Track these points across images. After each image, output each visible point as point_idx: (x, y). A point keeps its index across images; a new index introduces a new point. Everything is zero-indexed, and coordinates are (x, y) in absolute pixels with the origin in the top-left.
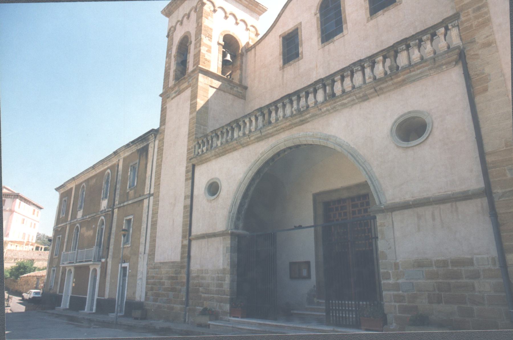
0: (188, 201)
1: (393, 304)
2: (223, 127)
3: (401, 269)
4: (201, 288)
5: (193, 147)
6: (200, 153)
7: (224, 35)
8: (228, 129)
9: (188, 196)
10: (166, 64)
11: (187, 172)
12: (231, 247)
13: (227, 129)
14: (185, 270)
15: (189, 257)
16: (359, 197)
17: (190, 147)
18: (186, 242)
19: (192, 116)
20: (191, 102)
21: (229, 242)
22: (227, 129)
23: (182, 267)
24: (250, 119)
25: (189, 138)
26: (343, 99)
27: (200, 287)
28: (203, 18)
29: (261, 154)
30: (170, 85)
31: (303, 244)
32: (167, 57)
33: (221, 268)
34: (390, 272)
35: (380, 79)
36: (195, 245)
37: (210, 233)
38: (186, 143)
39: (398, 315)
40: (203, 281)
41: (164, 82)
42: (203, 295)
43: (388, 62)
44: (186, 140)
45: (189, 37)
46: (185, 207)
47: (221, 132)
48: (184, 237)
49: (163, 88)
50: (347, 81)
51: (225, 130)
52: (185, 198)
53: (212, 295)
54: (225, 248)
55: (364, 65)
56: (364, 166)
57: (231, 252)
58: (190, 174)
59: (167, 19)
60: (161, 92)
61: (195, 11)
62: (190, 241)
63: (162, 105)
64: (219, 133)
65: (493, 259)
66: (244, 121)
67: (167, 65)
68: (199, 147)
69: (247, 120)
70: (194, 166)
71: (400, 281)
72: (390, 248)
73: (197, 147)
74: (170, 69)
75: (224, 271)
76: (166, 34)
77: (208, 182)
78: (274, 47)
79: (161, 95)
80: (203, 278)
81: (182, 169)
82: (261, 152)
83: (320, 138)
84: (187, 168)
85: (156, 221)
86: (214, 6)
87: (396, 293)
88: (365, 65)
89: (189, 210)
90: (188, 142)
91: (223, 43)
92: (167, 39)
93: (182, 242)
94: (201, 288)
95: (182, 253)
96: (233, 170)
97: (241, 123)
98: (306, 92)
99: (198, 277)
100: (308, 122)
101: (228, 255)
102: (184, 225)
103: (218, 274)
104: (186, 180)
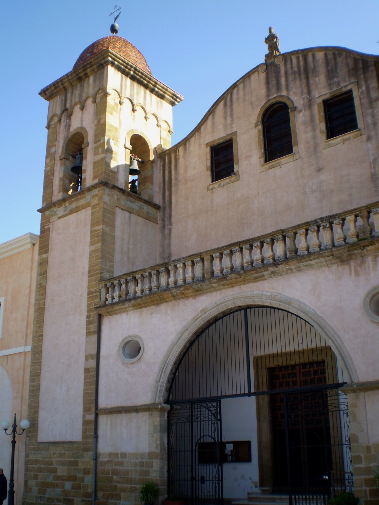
0: (93, 363)
1: (364, 488)
2: (144, 270)
3: (373, 453)
4: (115, 477)
5: (98, 290)
6: (109, 301)
7: (131, 136)
8: (153, 272)
9: (92, 356)
10: (46, 167)
11: (89, 323)
12: (160, 425)
13: (150, 273)
14: (91, 454)
15: (96, 436)
16: (311, 364)
17: (93, 290)
18: (92, 417)
19: (93, 248)
20: (91, 227)
21: (158, 419)
22: (150, 273)
23: (86, 450)
24: (184, 264)
25: (90, 276)
26: (310, 260)
27: (115, 475)
28: (107, 113)
29: (201, 311)
30: (55, 199)
31: (243, 418)
32: (47, 157)
33: (147, 451)
34: (362, 455)
35: (353, 245)
36: (103, 420)
37: (128, 407)
38: (85, 284)
39: (369, 499)
40: (118, 468)
41: (44, 193)
42: (119, 485)
43: (360, 221)
44: (86, 279)
45: (84, 135)
46: (87, 370)
47: (142, 275)
48: (86, 410)
49: (43, 201)
50: (312, 235)
51: (147, 274)
52: (87, 358)
53: (133, 485)
54: (152, 427)
55: (333, 221)
56: (332, 338)
57: (161, 432)
58: (94, 327)
59: (47, 102)
60: (40, 207)
61: (94, 101)
62: (97, 415)
63: (42, 224)
64: (138, 276)
65: (32, 236)
66: (176, 266)
67: (48, 168)
68: (108, 292)
69: (180, 265)
70: (100, 317)
71: (372, 465)
72: (363, 431)
73: (103, 291)
74: (53, 174)
75: (151, 455)
76: (46, 124)
77: (123, 340)
78: (197, 162)
79: (39, 211)
80: (120, 464)
81: (79, 320)
82: (201, 309)
83: (280, 301)
84: (88, 317)
85: (38, 386)
86: (145, 112)
87: (367, 477)
88: (334, 222)
89: (93, 376)
90: (89, 282)
91: (130, 147)
92: (47, 130)
93: (84, 416)
94: (115, 477)
95: (85, 431)
96: (164, 329)
97: (171, 268)
98: (261, 242)
99: (108, 462)
100: (266, 279)
101: (157, 436)
102: (86, 394)
103: (142, 458)
104: (88, 334)
